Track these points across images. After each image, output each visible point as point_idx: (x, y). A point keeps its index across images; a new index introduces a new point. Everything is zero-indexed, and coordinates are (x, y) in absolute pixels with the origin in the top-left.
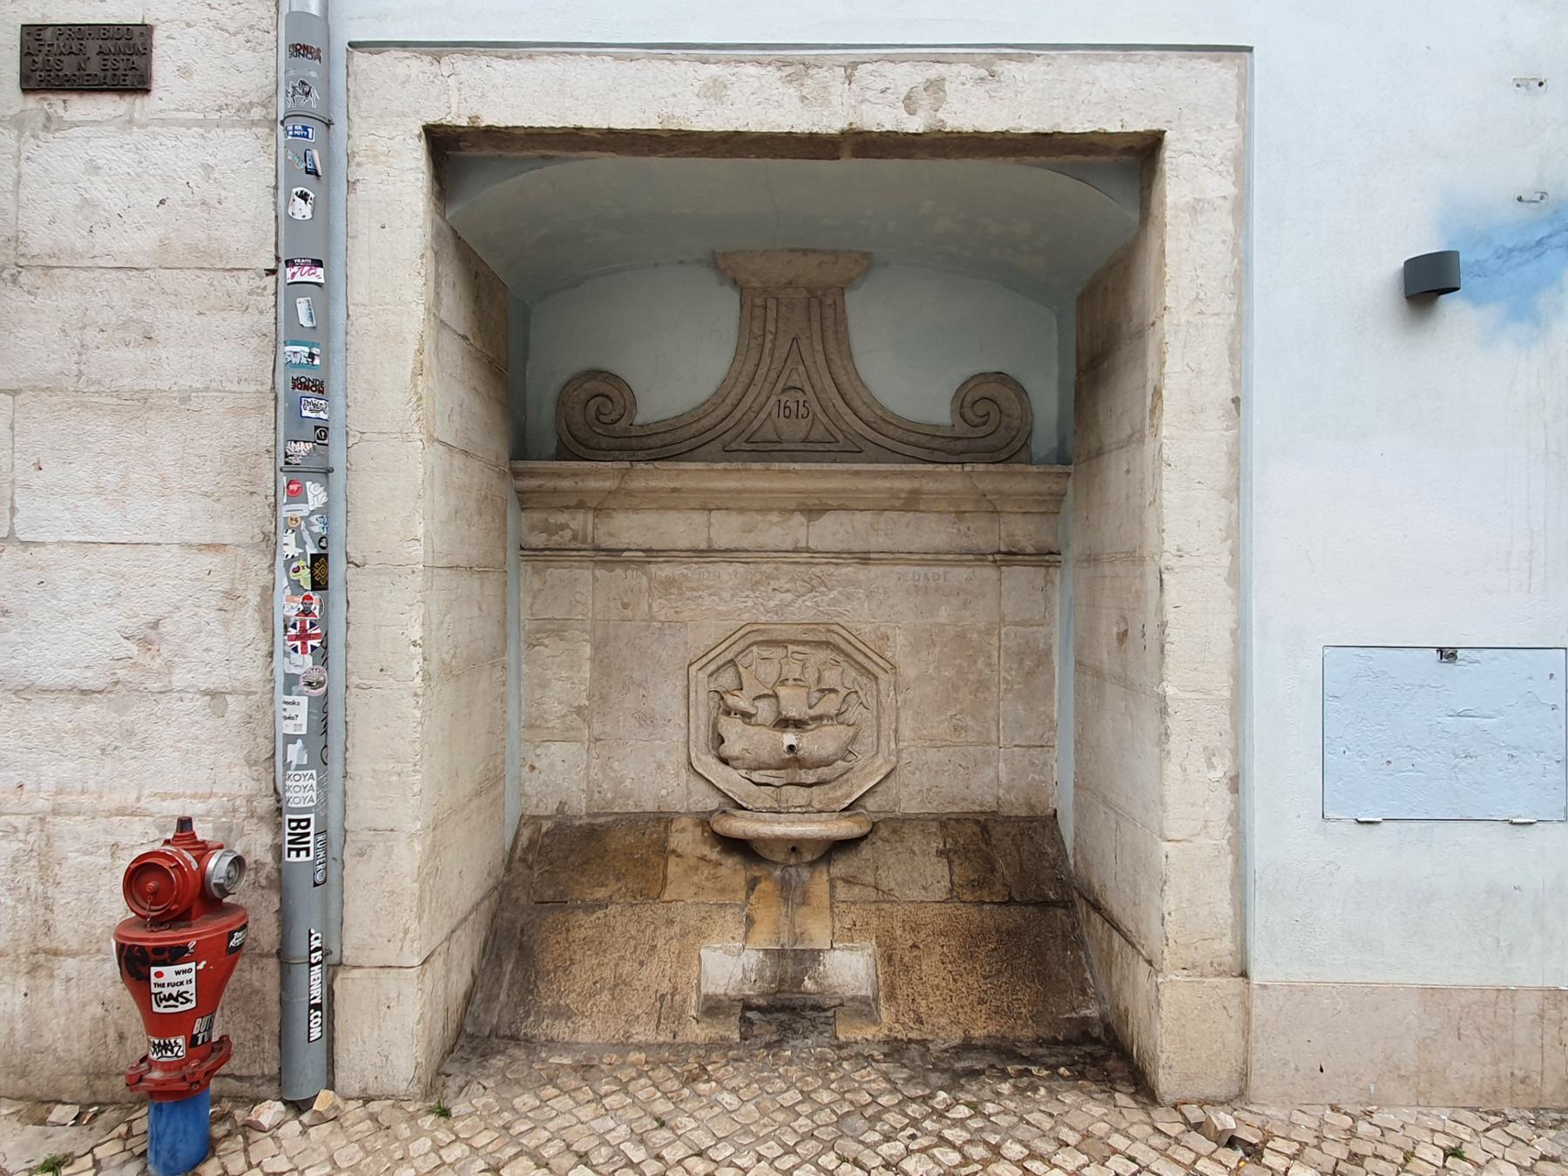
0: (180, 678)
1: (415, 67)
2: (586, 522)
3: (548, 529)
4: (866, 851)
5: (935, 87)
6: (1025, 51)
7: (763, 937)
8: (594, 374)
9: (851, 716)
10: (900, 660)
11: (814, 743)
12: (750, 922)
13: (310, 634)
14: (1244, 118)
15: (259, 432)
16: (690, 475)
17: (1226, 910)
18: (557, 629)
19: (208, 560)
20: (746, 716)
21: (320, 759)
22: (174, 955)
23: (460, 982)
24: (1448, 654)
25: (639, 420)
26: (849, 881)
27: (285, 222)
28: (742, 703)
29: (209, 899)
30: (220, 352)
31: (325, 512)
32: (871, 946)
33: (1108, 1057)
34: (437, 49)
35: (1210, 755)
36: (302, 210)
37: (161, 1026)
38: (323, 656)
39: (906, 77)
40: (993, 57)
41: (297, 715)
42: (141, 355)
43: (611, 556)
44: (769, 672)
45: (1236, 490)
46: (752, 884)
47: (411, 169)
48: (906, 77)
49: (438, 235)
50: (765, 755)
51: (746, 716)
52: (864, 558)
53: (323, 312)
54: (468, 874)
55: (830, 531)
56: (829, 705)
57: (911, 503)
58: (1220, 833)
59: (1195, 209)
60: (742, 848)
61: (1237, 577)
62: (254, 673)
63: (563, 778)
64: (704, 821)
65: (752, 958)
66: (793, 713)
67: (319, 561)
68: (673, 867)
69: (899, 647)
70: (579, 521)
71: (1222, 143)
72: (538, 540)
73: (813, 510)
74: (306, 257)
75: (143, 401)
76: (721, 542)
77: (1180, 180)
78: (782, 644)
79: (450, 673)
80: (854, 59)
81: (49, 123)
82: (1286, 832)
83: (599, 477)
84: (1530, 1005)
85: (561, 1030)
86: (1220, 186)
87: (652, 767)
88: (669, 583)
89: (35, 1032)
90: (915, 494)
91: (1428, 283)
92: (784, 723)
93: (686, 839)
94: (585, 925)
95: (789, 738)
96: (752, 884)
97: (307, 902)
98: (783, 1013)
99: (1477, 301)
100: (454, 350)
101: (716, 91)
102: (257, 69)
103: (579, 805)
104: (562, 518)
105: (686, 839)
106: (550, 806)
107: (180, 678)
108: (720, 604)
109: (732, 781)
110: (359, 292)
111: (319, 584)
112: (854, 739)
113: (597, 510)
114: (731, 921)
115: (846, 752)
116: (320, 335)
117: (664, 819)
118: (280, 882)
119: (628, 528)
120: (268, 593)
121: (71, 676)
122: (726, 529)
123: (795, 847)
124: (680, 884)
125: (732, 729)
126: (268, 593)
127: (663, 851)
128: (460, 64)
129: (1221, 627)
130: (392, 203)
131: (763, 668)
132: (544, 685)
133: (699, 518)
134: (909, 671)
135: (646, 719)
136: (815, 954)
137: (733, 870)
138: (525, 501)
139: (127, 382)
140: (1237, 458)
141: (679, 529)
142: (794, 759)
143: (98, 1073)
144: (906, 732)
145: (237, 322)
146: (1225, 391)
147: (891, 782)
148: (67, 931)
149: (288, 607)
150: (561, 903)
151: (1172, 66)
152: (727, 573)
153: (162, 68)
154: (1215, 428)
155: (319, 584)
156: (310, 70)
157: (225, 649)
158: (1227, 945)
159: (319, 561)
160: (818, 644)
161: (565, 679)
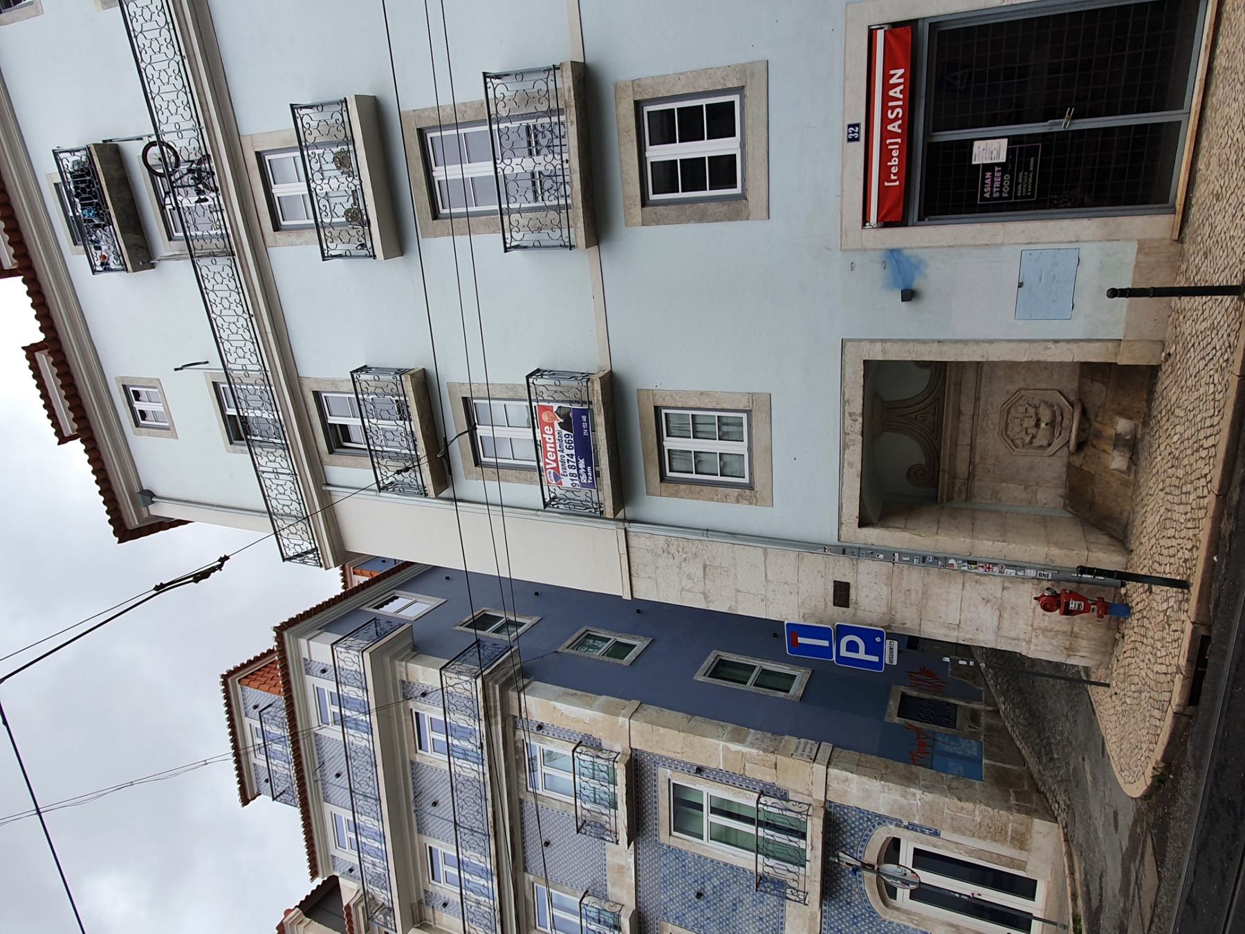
0: (999, 595)
1: (844, 528)
2: (898, 99)
3: (960, 491)
4: (1087, 406)
5: (850, 414)
6: (843, 394)
7: (1109, 448)
8: (908, 475)
9: (1036, 402)
10: (1017, 387)
11: (1045, 415)
12: (1104, 451)
13: (989, 566)
14: (860, 340)
15: (934, 571)
16: (945, 453)
17: (1098, 344)
18: (995, 493)
19: (967, 585)
20: (1033, 437)
21: (1023, 568)
22: (1067, 604)
23: (1106, 539)
24: (1020, 285)
25: (923, 462)
26: (1097, 416)
27: (884, 560)
28: (1028, 439)
29: (1055, 596)
30: (913, 578)
31: (956, 560)
32: (1118, 418)
33: (1150, 374)
34: (840, 524)
35: (1047, 348)
36: (881, 556)
37: (1087, 610)
38: (995, 564)
39: (848, 421)
40: (844, 402)
41: (1011, 572)
42: (913, 593)
43: (971, 475)
44: (1017, 429)
45: (965, 342)
46: (1094, 446)
47: (867, 532)
48: (848, 421)
49: (882, 526)
50: (1048, 433)
51: (1033, 437)
52: (977, 399)
53: (906, 554)
54: (1070, 532)
55: (967, 409)
56: (1032, 411)
57: (959, 384)
58: (1071, 346)
59: (884, 352)
60: (1080, 446)
61: (991, 342)
62: (999, 580)
63: (1050, 496)
64: (1071, 454)
65: (1116, 453)
66: (1033, 423)
67: (969, 562)
68: (1085, 468)
69: (1012, 388)
70: (958, 483)
71: (867, 345)
72: (964, 496)
73: (959, 413)
74: (890, 555)
75: (925, 594)
76: (969, 441)
77: (877, 354)
78: (1007, 424)
79: (1004, 534)
80: (844, 433)
81: (856, 603)
82: (1076, 328)
83: (944, 479)
84: (1142, 257)
85: (1125, 514)
86: (879, 346)
87: (1050, 467)
88: (982, 458)
89: (1095, 639)
90: (956, 384)
91: (909, 295)
92: (1037, 425)
93: (1077, 461)
94: (1098, 499)
95: (1043, 425)
96: (1094, 446)
97: (1062, 575)
98: (1132, 447)
99: (913, 279)
100: (911, 524)
101: (851, 465)
102: (844, 561)
103: (1061, 491)
104: (956, 489)
105: (1077, 461)
106: (1061, 501)
107: (999, 595)
108: (991, 442)
109: (1057, 443)
110: (899, 546)
111: (975, 563)
112: (1046, 403)
113: (954, 477)
114: (1104, 456)
115: (1050, 406)
116: (912, 556)
117: (1069, 466)
118: (1058, 581)
119: (962, 468)
120: (977, 574)
121: (996, 618)
122: (964, 440)
123: (1081, 430)
124: (1090, 468)
125: (1037, 442)
126: (977, 574)
127: (1080, 469)
128: (844, 518)
129: (1006, 346)
130: (873, 536)
131: (1015, 429)
132: (1015, 498)
133: (959, 448)
134: (1022, 385)
135: (1031, 468)
136: (1116, 435)
137: (1089, 450)
138: (950, 499)
139: (920, 596)
140: (956, 342)
141: (963, 454)
142: (1052, 424)
143: (1109, 628)
144: (1045, 386)
145: (905, 572)
146: (936, 345)
147: (1064, 392)
148: (1067, 628)
149: (981, 570)
150: (1092, 504)
151: (847, 358)
152: (980, 440)
153: (844, 580)
154: (945, 348)
155: (975, 563)
156: (848, 551)
157: (992, 586)
158: (1110, 345)
159: (969, 562)
160: (1008, 412)
161: (1013, 492)
